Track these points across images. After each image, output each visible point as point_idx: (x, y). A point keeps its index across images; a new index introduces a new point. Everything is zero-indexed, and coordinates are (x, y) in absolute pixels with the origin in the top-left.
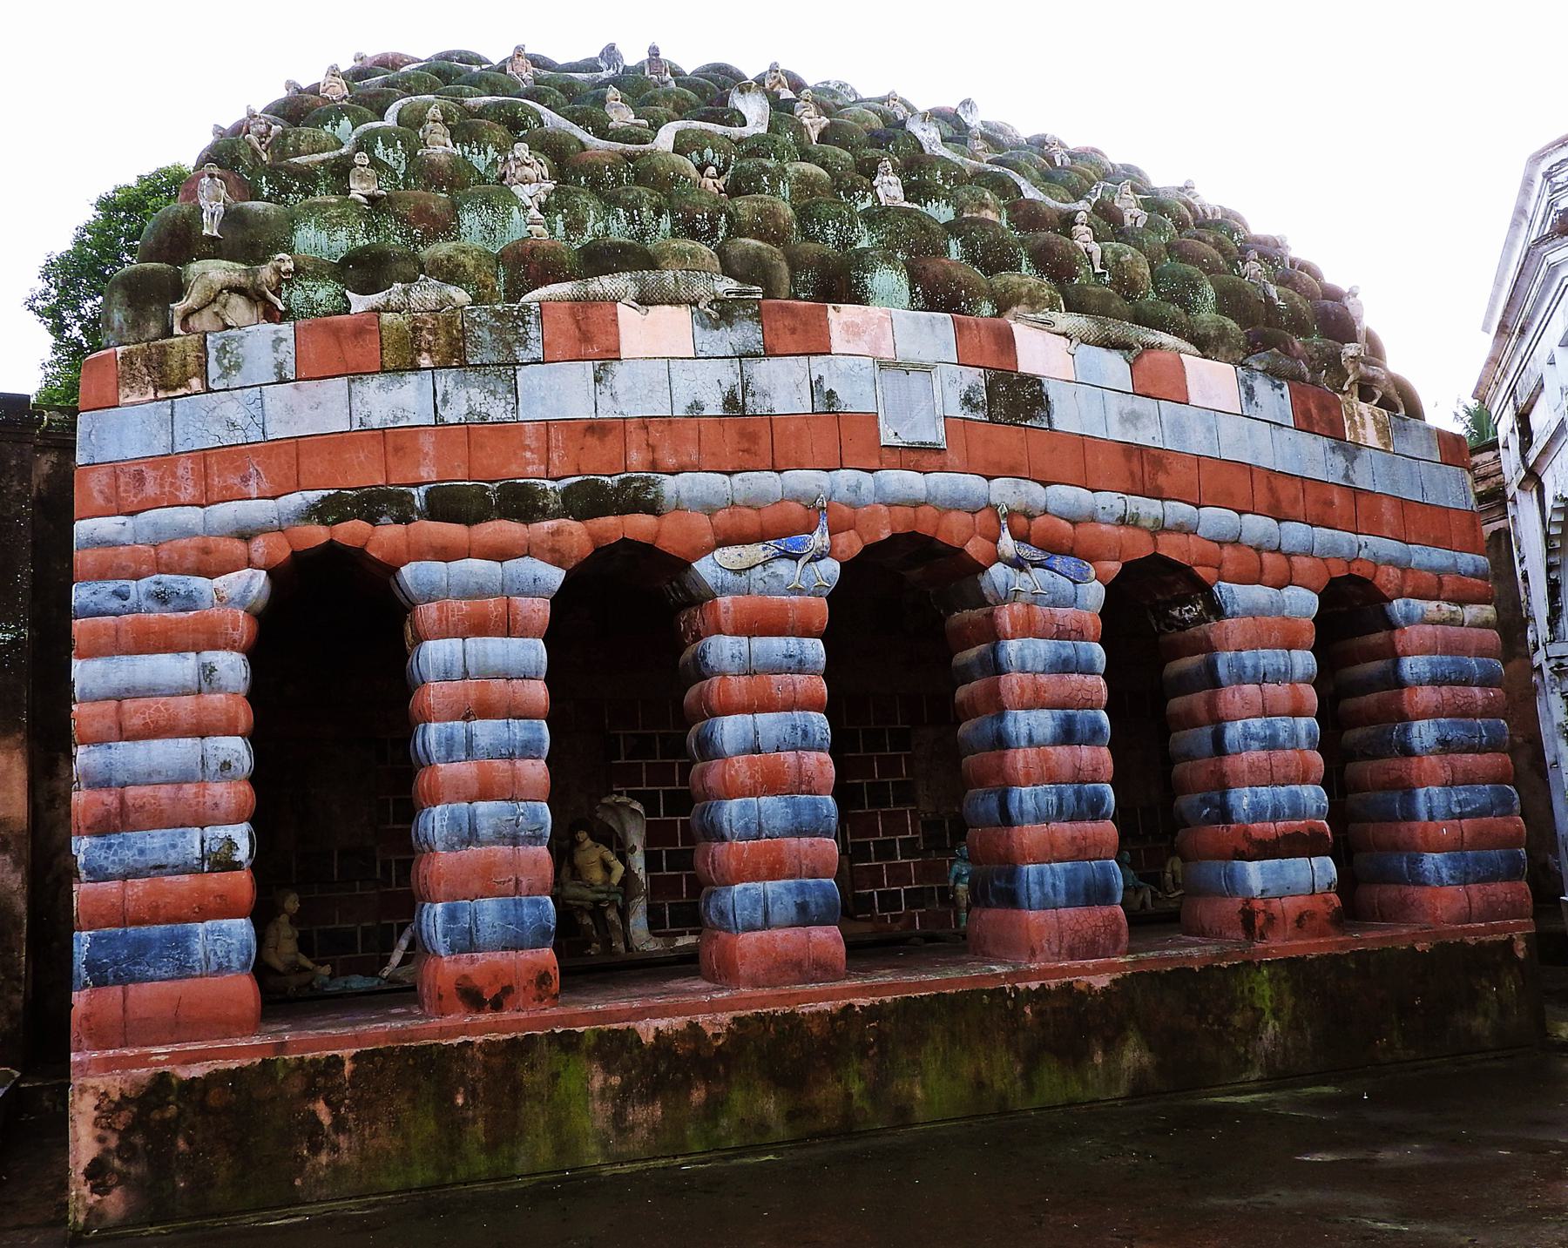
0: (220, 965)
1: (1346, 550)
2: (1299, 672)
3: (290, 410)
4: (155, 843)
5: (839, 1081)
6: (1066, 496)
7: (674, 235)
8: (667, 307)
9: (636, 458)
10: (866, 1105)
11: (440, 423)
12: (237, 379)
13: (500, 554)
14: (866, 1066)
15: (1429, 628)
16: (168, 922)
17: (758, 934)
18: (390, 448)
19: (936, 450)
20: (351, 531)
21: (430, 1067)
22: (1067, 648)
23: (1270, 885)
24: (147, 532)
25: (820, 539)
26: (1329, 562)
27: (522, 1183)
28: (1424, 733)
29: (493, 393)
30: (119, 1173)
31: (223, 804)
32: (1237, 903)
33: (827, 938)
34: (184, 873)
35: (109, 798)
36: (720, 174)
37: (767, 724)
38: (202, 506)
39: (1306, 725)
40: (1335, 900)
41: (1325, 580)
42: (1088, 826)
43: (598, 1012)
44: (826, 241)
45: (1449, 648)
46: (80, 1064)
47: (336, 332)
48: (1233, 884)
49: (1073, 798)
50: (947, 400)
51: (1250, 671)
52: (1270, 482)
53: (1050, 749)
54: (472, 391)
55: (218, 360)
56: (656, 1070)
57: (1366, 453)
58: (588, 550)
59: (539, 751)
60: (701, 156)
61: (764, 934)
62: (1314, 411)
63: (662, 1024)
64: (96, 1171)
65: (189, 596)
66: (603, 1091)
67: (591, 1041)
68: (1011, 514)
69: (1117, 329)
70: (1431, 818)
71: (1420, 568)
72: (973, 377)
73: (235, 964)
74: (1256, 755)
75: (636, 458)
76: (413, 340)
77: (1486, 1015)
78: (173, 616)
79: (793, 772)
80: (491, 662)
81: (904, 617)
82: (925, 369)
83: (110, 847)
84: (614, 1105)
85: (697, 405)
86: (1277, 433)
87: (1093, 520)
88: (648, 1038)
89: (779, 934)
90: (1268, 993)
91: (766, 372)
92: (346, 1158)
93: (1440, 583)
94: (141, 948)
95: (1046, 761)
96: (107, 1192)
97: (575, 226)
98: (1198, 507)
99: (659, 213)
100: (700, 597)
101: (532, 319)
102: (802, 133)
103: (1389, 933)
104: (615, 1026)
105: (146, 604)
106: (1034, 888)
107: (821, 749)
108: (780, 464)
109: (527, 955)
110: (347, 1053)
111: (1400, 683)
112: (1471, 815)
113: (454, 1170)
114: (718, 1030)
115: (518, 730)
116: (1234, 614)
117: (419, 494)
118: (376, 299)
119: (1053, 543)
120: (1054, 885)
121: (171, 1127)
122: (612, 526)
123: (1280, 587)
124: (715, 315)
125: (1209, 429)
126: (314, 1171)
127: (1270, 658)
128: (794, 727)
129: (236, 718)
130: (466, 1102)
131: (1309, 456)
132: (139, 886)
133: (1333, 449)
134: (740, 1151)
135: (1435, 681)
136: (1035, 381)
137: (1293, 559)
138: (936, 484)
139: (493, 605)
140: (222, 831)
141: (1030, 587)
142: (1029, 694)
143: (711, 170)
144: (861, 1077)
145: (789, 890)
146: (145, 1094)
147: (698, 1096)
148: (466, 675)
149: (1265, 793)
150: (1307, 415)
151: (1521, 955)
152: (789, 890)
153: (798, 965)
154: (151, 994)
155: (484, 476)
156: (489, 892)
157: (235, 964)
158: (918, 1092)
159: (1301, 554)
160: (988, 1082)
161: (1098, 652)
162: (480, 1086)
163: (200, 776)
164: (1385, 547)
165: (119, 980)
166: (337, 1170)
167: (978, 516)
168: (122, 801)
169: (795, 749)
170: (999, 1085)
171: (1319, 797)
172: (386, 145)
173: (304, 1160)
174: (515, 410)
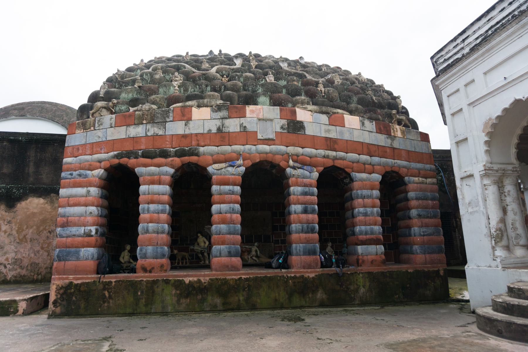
2: (374, 195)
3: (112, 133)
4: (74, 230)
6: (308, 150)
7: (211, 91)
9: (194, 143)
11: (147, 135)
12: (101, 127)
13: (159, 166)
14: (245, 293)
15: (416, 185)
16: (76, 247)
19: (273, 140)
20: (124, 161)
21: (133, 285)
22: (307, 189)
25: (240, 162)
28: (414, 212)
29: (160, 129)
31: (90, 222)
32: (355, 257)
33: (237, 261)
35: (65, 219)
36: (227, 77)
37: (226, 208)
40: (383, 257)
47: (125, 117)
48: (355, 253)
49: (306, 228)
51: (360, 196)
54: (155, 128)
55: (98, 123)
58: (180, 164)
61: (219, 258)
62: (382, 128)
63: (191, 279)
64: (55, 303)
66: (175, 294)
67: (173, 282)
68: (292, 155)
71: (413, 168)
72: (284, 122)
75: (194, 143)
78: (82, 179)
80: (155, 191)
81: (264, 183)
82: (271, 120)
85: (210, 130)
86: (371, 134)
89: (223, 259)
90: (361, 281)
91: (227, 122)
94: (69, 253)
96: (57, 307)
98: (347, 153)
99: (207, 86)
105: (77, 177)
107: (237, 213)
108: (231, 144)
109: (159, 260)
110: (113, 280)
112: (427, 235)
115: (160, 207)
116: (356, 181)
117: (140, 152)
118: (135, 108)
119: (303, 163)
120: (299, 250)
122: (186, 159)
125: (351, 133)
127: (365, 192)
128: (230, 208)
131: (381, 140)
132: (69, 239)
133: (387, 138)
135: (417, 199)
136: (301, 122)
139: (156, 177)
140: (89, 228)
143: (225, 76)
144: (243, 296)
146: (67, 286)
147: (200, 297)
148: (149, 194)
149: (363, 228)
150: (380, 129)
151: (442, 274)
153: (227, 266)
154: (70, 264)
157: (90, 258)
158: (259, 301)
161: (315, 190)
162: (144, 291)
165: (64, 260)
168: (67, 220)
169: (230, 213)
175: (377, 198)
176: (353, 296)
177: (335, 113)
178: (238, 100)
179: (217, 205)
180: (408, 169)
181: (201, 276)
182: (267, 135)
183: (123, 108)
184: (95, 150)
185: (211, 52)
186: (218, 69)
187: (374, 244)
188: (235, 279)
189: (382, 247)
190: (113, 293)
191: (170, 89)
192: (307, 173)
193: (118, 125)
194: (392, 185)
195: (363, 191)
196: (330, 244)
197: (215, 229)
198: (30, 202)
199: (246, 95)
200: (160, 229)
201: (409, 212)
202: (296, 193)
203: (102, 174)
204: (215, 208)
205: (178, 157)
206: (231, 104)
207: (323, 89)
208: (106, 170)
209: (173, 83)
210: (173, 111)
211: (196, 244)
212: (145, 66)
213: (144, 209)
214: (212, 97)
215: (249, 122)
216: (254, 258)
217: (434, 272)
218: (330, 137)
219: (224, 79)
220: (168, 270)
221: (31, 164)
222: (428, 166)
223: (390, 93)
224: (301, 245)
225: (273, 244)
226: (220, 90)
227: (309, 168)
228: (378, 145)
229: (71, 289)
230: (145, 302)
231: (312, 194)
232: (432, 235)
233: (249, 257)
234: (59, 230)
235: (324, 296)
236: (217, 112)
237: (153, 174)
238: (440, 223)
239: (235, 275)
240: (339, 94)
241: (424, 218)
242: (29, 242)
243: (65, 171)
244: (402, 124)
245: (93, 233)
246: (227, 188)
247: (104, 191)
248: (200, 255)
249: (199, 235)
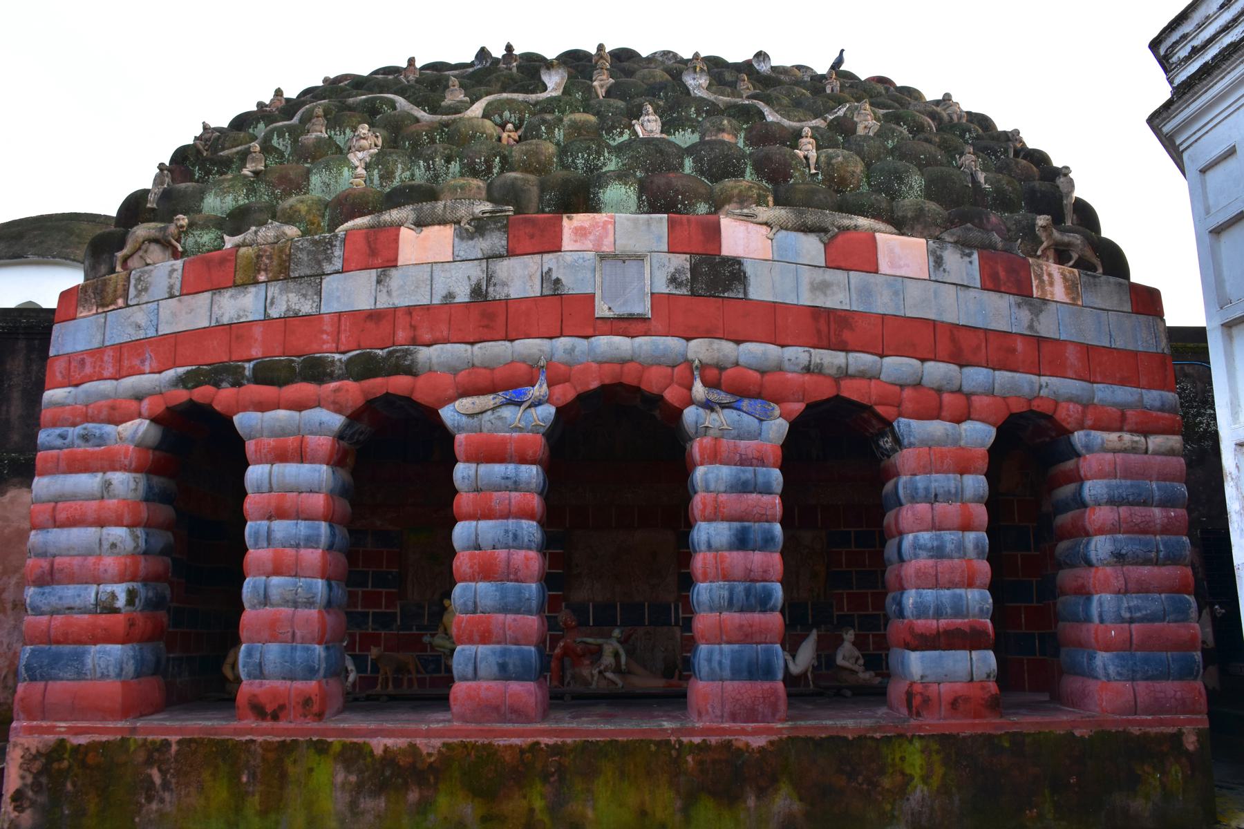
3: (174, 315)
4: (70, 594)
5: (525, 797)
6: (755, 351)
7: (462, 175)
8: (436, 228)
9: (401, 335)
10: (546, 819)
12: (145, 298)
13: (299, 406)
15: (1109, 456)
17: (469, 683)
19: (642, 319)
20: (202, 393)
21: (226, 754)
22: (748, 473)
23: (928, 672)
25: (539, 390)
28: (1100, 547)
29: (304, 296)
31: (110, 571)
33: (525, 691)
36: (517, 128)
37: (495, 530)
39: (976, 539)
40: (993, 687)
41: (1003, 415)
42: (757, 616)
43: (344, 729)
44: (576, 168)
45: (1128, 473)
46: (16, 728)
47: (208, 263)
49: (743, 594)
50: (656, 280)
51: (921, 492)
53: (726, 554)
54: (291, 295)
55: (136, 286)
58: (360, 402)
59: (317, 542)
60: (501, 116)
61: (473, 684)
62: (1002, 274)
63: (389, 742)
64: (18, 797)
65: (101, 437)
66: (343, 784)
67: (337, 748)
68: (703, 367)
69: (812, 217)
70: (1102, 621)
72: (681, 261)
74: (923, 562)
76: (256, 264)
81: (616, 453)
82: (639, 258)
85: (450, 295)
86: (962, 293)
88: (379, 751)
89: (484, 684)
91: (504, 268)
92: (168, 808)
94: (56, 659)
95: (722, 562)
96: (22, 811)
97: (387, 176)
98: (923, 360)
99: (448, 160)
100: (445, 436)
101: (338, 243)
102: (590, 92)
104: (355, 740)
105: (78, 442)
107: (529, 548)
109: (299, 685)
110: (174, 738)
111: (1083, 505)
112: (1141, 620)
114: (430, 750)
115: (303, 527)
116: (911, 445)
117: (249, 366)
118: (238, 239)
119: (737, 388)
120: (720, 663)
123: (959, 422)
124: (471, 229)
125: (896, 293)
128: (507, 531)
130: (248, 781)
131: (999, 312)
132: (59, 618)
133: (1019, 305)
135: (1113, 502)
136: (736, 262)
137: (973, 398)
138: (640, 346)
141: (717, 424)
142: (709, 511)
143: (510, 126)
144: (543, 797)
146: (51, 752)
147: (413, 796)
149: (929, 595)
151: (1191, 748)
153: (497, 709)
154: (59, 688)
156: (274, 638)
157: (112, 674)
158: (590, 814)
159: (982, 394)
161: (776, 475)
162: (258, 771)
163: (98, 552)
165: (42, 678)
166: (162, 814)
167: (676, 369)
169: (507, 547)
171: (983, 599)
172: (279, 137)
173: (142, 806)
174: (319, 306)
175: (977, 500)
176: (888, 807)
177: (847, 229)
178: (541, 199)
179: (467, 523)
180: (1087, 405)
182: (625, 303)
183: (207, 238)
184: (126, 363)
185: (483, 53)
186: (489, 104)
187: (963, 648)
188: (520, 747)
189: (990, 656)
192: (749, 421)
193: (189, 288)
194: (1029, 456)
195: (934, 476)
196: (849, 636)
198: (12, 501)
201: (1088, 543)
202: (712, 487)
203: (145, 433)
204: (462, 532)
205: (356, 380)
206: (515, 213)
208: (155, 420)
209: (351, 156)
210: (344, 241)
211: (441, 629)
213: (256, 534)
214: (463, 194)
215: (572, 267)
216: (609, 675)
217: (1162, 738)
218: (829, 305)
219: (505, 135)
220: (327, 715)
221: (16, 394)
223: (1039, 158)
224: (726, 647)
225: (677, 630)
226: (489, 168)
227: (758, 405)
228: (986, 331)
229: (61, 759)
233: (595, 672)
234: (30, 592)
235: (797, 806)
236: (472, 239)
237: (282, 433)
238: (1191, 579)
240: (868, 166)
241: (1136, 564)
242: (9, 612)
243: (46, 427)
244: (1070, 258)
245: (121, 602)
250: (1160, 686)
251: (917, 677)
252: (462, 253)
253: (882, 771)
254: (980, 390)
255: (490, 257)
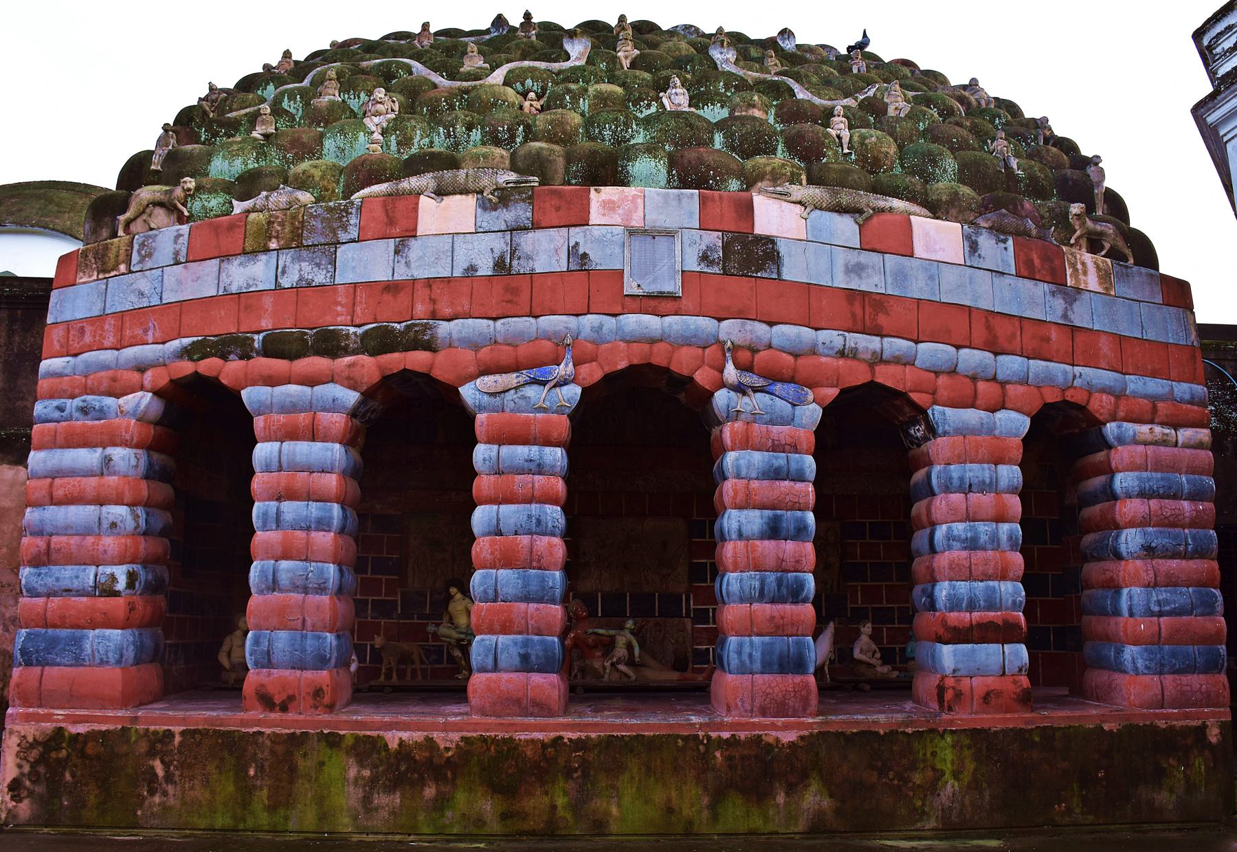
0: (102, 660)
1: (1060, 379)
2: (1003, 483)
3: (179, 282)
4: (66, 574)
5: (547, 794)
6: (786, 333)
7: (484, 144)
8: (458, 197)
9: (420, 309)
10: (569, 816)
11: (278, 287)
12: (149, 264)
14: (571, 785)
15: (1141, 448)
16: (72, 627)
17: (489, 675)
18: (242, 307)
19: (672, 297)
20: (209, 366)
21: (232, 747)
22: (780, 459)
23: (961, 666)
24: (81, 367)
25: (565, 369)
26: (1044, 391)
27: (293, 837)
28: (1130, 540)
29: (318, 265)
30: (28, 789)
31: (110, 552)
32: (934, 681)
33: (548, 684)
34: (83, 596)
35: (41, 543)
36: (539, 97)
37: (517, 513)
38: (118, 349)
39: (1010, 530)
40: (1025, 681)
41: (1036, 405)
42: (788, 607)
43: (356, 721)
45: (1158, 466)
46: (11, 715)
47: (216, 229)
48: (934, 665)
49: (774, 585)
50: (686, 257)
51: (956, 482)
52: (987, 321)
53: (758, 543)
54: (303, 264)
55: (139, 252)
56: (398, 769)
57: (1086, 296)
58: (376, 378)
61: (493, 675)
62: (1037, 262)
63: (405, 735)
65: (101, 410)
66: (356, 779)
67: (349, 741)
68: (735, 348)
69: (846, 197)
70: (1131, 615)
71: (1135, 395)
72: (714, 239)
73: (112, 660)
75: (420, 309)
77: (1171, 790)
78: (90, 423)
79: (526, 551)
80: (298, 459)
81: (642, 442)
82: (669, 234)
83: (39, 575)
84: (365, 791)
85: (472, 268)
87: (814, 353)
88: (393, 745)
89: (505, 676)
90: (949, 757)
91: (528, 241)
92: (172, 801)
93: (1154, 409)
94: (53, 642)
96: (20, 801)
97: (405, 142)
98: (917, 342)
99: (470, 128)
100: (465, 417)
101: (354, 211)
103: (1078, 713)
104: (368, 733)
105: (76, 415)
106: (733, 656)
107: (553, 535)
109: (308, 674)
110: (177, 729)
111: (1114, 497)
112: (1169, 614)
113: (245, 821)
115: (314, 509)
116: (945, 433)
117: (258, 339)
118: (248, 204)
119: (770, 372)
120: (750, 655)
121: (62, 764)
122: (395, 360)
123: (993, 411)
124: (495, 200)
125: (931, 278)
126: (150, 807)
127: (976, 472)
128: (530, 517)
129: (123, 493)
131: (1033, 300)
132: (56, 602)
133: (1053, 294)
134: (460, 837)
135: (1144, 494)
136: (770, 240)
138: (670, 325)
139: (302, 418)
140: (109, 570)
141: (749, 408)
143: (532, 95)
144: (565, 793)
145: (516, 644)
146: (49, 740)
147: (430, 792)
148: (280, 469)
149: (963, 587)
150: (1029, 264)
151: (1214, 740)
152: (516, 644)
153: (518, 702)
155: (306, 324)
157: (112, 660)
158: (614, 810)
159: (1016, 383)
160: (677, 809)
161: (809, 463)
162: (266, 764)
163: (97, 530)
164: (1104, 377)
165: (39, 663)
166: (165, 808)
167: (707, 351)
168: (49, 545)
169: (530, 533)
170: (687, 812)
171: (1016, 592)
173: (144, 798)
175: (1012, 490)
181: (434, 726)
182: (655, 281)
183: (215, 202)
184: (128, 333)
186: (510, 72)
188: (542, 742)
189: (1023, 649)
190: (176, 768)
191: (356, 139)
193: (194, 256)
195: (968, 465)
197: (481, 584)
199: (594, 153)
200: (313, 581)
201: (1118, 536)
202: (744, 473)
203: (147, 407)
204: (481, 516)
205: (371, 355)
207: (846, 134)
208: (157, 393)
211: (446, 619)
212: (290, 73)
215: (600, 241)
216: (622, 667)
217: (1187, 731)
218: (863, 288)
222: (1185, 386)
223: (1068, 146)
224: (756, 639)
225: (688, 622)
226: (513, 137)
227: (790, 389)
230: (269, 798)
231: (800, 477)
232: (1190, 613)
233: (608, 664)
234: (25, 572)
235: (826, 803)
236: (495, 210)
237: (291, 408)
238: (1218, 572)
239: (541, 729)
240: (900, 147)
244: (1102, 248)
245: (121, 585)
246: (521, 451)
247: (156, 456)
248: (457, 653)
249: (453, 590)
250: (1186, 679)
251: (949, 671)
252: (484, 224)
253: (913, 767)
254: (1015, 379)
255: (515, 229)
